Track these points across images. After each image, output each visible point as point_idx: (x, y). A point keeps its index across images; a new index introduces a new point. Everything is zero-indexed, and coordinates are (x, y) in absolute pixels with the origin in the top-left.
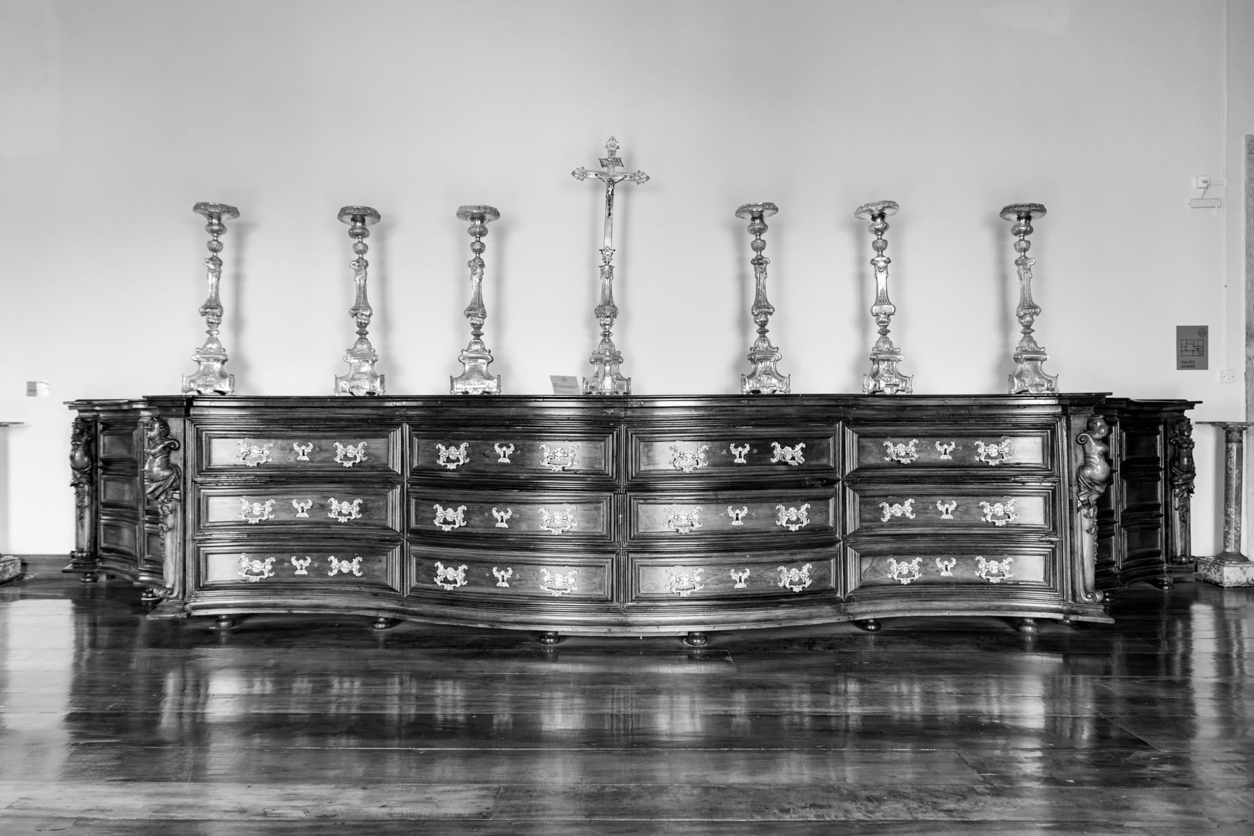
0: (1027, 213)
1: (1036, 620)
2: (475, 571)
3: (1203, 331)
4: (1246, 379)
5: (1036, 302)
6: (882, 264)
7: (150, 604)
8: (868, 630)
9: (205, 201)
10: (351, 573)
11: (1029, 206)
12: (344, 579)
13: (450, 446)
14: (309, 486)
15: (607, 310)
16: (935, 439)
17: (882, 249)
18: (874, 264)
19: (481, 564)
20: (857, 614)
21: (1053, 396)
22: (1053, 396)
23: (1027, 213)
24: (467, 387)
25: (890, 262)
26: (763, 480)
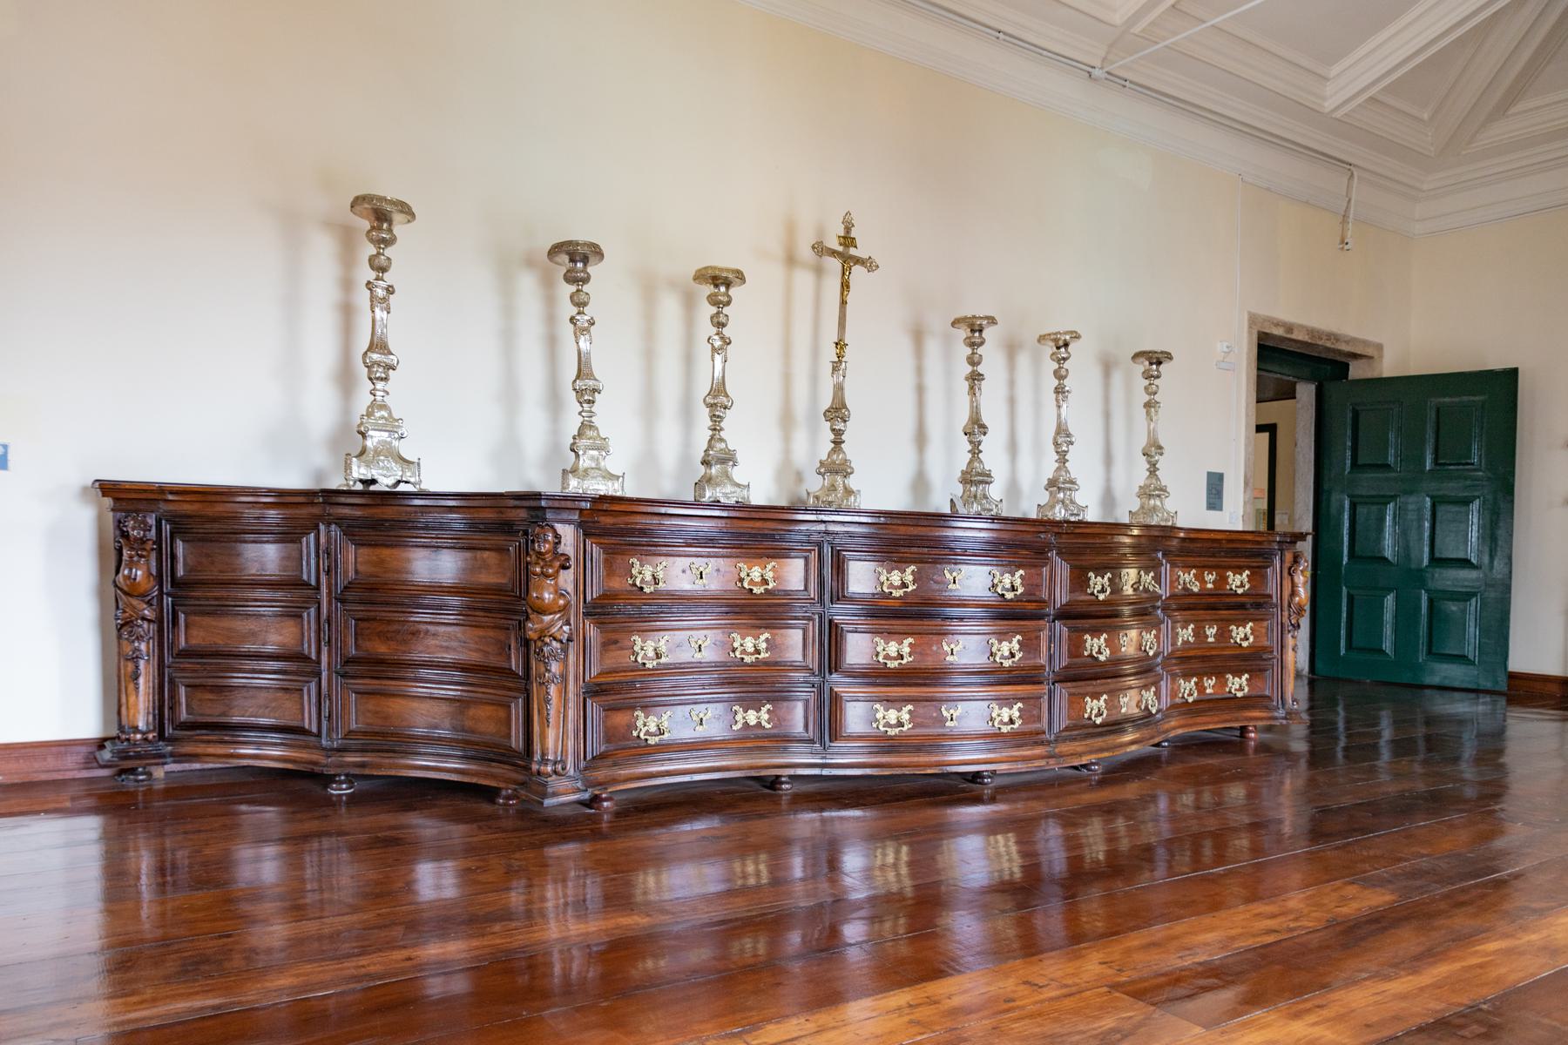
0: (1157, 359)
2: (921, 711)
3: (1220, 477)
4: (1243, 520)
6: (380, 293)
7: (344, 798)
8: (1163, 747)
9: (713, 265)
10: (759, 725)
12: (749, 733)
13: (893, 569)
15: (837, 412)
16: (1203, 569)
17: (383, 270)
18: (370, 289)
20: (1167, 731)
21: (993, 519)
22: (993, 519)
23: (1157, 359)
24: (374, 472)
25: (593, 324)
26: (1098, 613)
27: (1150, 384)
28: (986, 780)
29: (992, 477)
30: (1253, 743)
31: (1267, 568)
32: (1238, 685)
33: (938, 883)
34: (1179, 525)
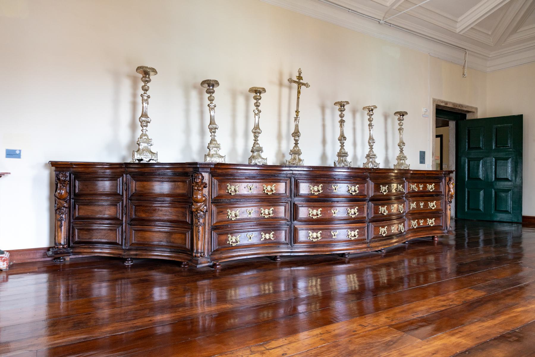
0: (402, 114)
1: (280, 256)
2: (324, 233)
3: (424, 153)
5: (404, 142)
6: (145, 98)
7: (130, 266)
10: (270, 239)
12: (267, 241)
13: (315, 186)
14: (317, 203)
17: (147, 90)
21: (348, 168)
23: (402, 114)
24: (142, 157)
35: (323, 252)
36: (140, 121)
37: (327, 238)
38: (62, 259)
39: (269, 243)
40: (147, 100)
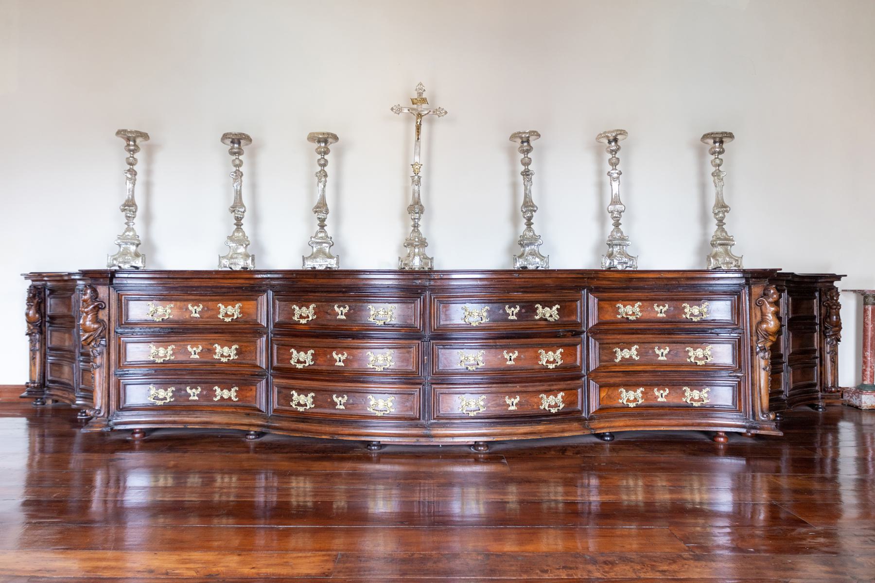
0: (721, 139)
1: (726, 433)
2: (320, 397)
5: (727, 203)
6: (615, 175)
7: (84, 421)
8: (605, 440)
10: (230, 398)
11: (722, 133)
13: (302, 306)
19: (325, 393)
23: (721, 139)
25: (621, 174)
27: (716, 158)
28: (373, 448)
29: (733, 241)
30: (722, 447)
31: (577, 301)
32: (552, 402)
33: (32, 516)
34: (435, 269)
35: (317, 433)
36: (522, 211)
37: (325, 408)
38: (39, 402)
39: (228, 406)
40: (618, 178)
